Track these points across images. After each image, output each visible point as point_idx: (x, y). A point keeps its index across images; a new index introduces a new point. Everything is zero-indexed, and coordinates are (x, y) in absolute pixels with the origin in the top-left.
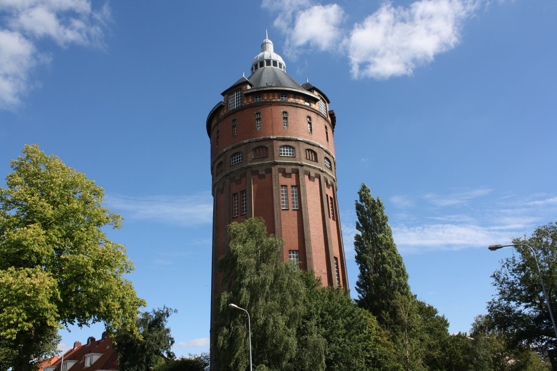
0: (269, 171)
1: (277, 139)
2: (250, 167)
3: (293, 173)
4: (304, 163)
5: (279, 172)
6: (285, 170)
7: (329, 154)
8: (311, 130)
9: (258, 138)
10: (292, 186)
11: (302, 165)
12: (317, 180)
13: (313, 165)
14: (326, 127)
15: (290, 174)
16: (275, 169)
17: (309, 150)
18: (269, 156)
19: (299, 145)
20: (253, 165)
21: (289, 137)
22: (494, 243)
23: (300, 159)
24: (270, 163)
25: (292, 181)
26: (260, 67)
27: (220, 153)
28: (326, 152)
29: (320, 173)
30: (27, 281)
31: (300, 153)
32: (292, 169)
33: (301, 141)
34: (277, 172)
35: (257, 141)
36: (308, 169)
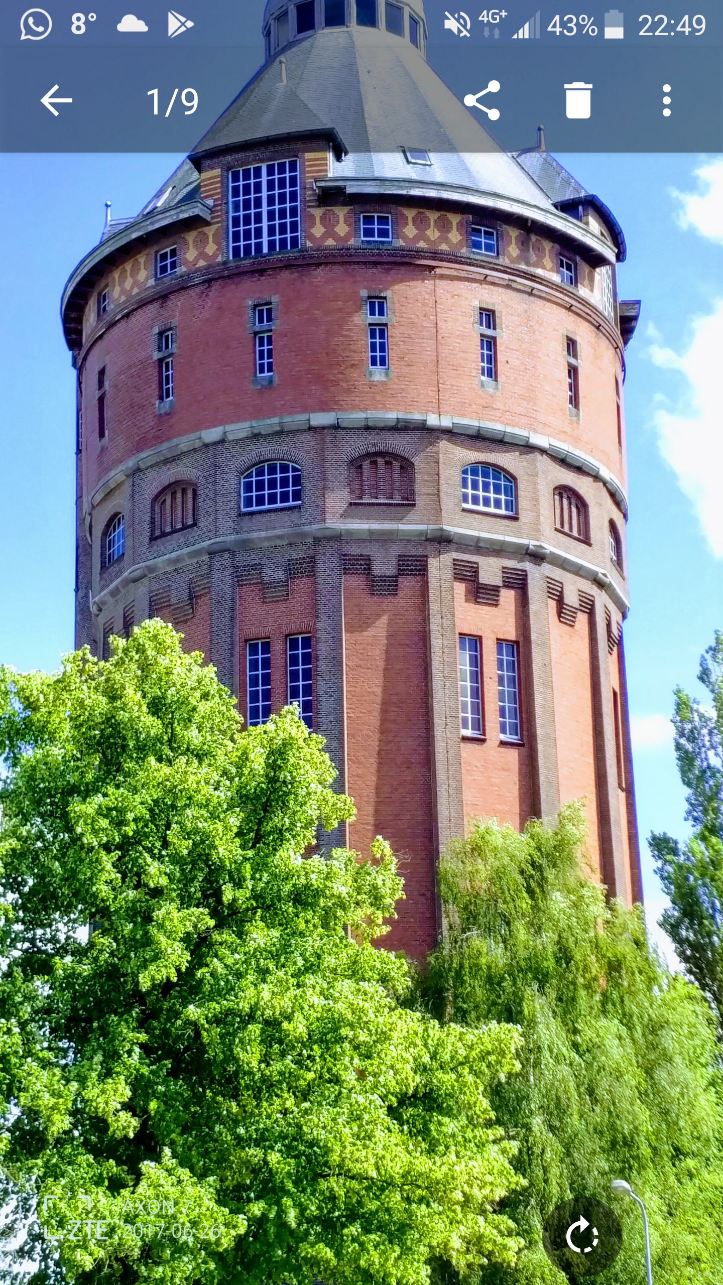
0: (414, 567)
1: (450, 434)
2: (337, 537)
3: (507, 585)
5: (458, 577)
6: (476, 571)
7: (580, 469)
8: (575, 400)
10: (500, 641)
11: (538, 557)
12: (582, 619)
14: (571, 345)
15: (496, 589)
16: (440, 567)
17: (372, 456)
18: (420, 501)
19: (533, 463)
20: (349, 532)
21: (499, 427)
22: (108, 373)
23: (536, 531)
24: (421, 533)
25: (496, 622)
28: (563, 461)
29: (594, 590)
30: (361, 1003)
31: (536, 500)
33: (543, 451)
34: (448, 574)
36: (557, 573)
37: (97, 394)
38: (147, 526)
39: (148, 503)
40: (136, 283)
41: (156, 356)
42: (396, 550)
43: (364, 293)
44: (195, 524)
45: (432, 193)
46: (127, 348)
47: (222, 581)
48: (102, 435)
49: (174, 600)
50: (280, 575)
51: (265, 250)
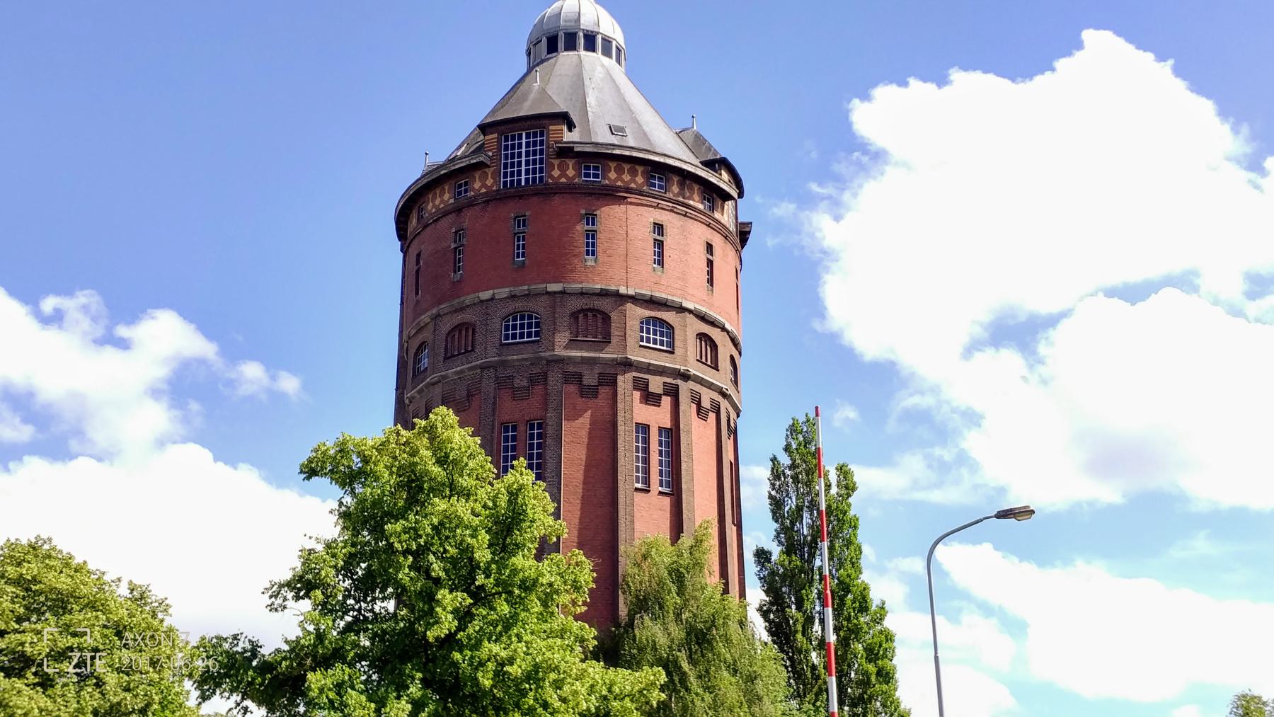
1: (635, 299)
2: (561, 360)
3: (666, 394)
5: (636, 388)
7: (713, 323)
8: (711, 281)
9: (590, 286)
11: (686, 377)
12: (712, 416)
14: (710, 248)
15: (660, 396)
16: (624, 381)
17: (585, 311)
18: (614, 340)
20: (570, 358)
24: (613, 359)
25: (659, 417)
26: (567, 49)
27: (468, 299)
33: (690, 311)
34: (630, 386)
35: (583, 294)
36: (698, 388)
40: (442, 202)
41: (453, 246)
42: (597, 370)
43: (583, 212)
47: (488, 385)
48: (417, 293)
50: (525, 383)
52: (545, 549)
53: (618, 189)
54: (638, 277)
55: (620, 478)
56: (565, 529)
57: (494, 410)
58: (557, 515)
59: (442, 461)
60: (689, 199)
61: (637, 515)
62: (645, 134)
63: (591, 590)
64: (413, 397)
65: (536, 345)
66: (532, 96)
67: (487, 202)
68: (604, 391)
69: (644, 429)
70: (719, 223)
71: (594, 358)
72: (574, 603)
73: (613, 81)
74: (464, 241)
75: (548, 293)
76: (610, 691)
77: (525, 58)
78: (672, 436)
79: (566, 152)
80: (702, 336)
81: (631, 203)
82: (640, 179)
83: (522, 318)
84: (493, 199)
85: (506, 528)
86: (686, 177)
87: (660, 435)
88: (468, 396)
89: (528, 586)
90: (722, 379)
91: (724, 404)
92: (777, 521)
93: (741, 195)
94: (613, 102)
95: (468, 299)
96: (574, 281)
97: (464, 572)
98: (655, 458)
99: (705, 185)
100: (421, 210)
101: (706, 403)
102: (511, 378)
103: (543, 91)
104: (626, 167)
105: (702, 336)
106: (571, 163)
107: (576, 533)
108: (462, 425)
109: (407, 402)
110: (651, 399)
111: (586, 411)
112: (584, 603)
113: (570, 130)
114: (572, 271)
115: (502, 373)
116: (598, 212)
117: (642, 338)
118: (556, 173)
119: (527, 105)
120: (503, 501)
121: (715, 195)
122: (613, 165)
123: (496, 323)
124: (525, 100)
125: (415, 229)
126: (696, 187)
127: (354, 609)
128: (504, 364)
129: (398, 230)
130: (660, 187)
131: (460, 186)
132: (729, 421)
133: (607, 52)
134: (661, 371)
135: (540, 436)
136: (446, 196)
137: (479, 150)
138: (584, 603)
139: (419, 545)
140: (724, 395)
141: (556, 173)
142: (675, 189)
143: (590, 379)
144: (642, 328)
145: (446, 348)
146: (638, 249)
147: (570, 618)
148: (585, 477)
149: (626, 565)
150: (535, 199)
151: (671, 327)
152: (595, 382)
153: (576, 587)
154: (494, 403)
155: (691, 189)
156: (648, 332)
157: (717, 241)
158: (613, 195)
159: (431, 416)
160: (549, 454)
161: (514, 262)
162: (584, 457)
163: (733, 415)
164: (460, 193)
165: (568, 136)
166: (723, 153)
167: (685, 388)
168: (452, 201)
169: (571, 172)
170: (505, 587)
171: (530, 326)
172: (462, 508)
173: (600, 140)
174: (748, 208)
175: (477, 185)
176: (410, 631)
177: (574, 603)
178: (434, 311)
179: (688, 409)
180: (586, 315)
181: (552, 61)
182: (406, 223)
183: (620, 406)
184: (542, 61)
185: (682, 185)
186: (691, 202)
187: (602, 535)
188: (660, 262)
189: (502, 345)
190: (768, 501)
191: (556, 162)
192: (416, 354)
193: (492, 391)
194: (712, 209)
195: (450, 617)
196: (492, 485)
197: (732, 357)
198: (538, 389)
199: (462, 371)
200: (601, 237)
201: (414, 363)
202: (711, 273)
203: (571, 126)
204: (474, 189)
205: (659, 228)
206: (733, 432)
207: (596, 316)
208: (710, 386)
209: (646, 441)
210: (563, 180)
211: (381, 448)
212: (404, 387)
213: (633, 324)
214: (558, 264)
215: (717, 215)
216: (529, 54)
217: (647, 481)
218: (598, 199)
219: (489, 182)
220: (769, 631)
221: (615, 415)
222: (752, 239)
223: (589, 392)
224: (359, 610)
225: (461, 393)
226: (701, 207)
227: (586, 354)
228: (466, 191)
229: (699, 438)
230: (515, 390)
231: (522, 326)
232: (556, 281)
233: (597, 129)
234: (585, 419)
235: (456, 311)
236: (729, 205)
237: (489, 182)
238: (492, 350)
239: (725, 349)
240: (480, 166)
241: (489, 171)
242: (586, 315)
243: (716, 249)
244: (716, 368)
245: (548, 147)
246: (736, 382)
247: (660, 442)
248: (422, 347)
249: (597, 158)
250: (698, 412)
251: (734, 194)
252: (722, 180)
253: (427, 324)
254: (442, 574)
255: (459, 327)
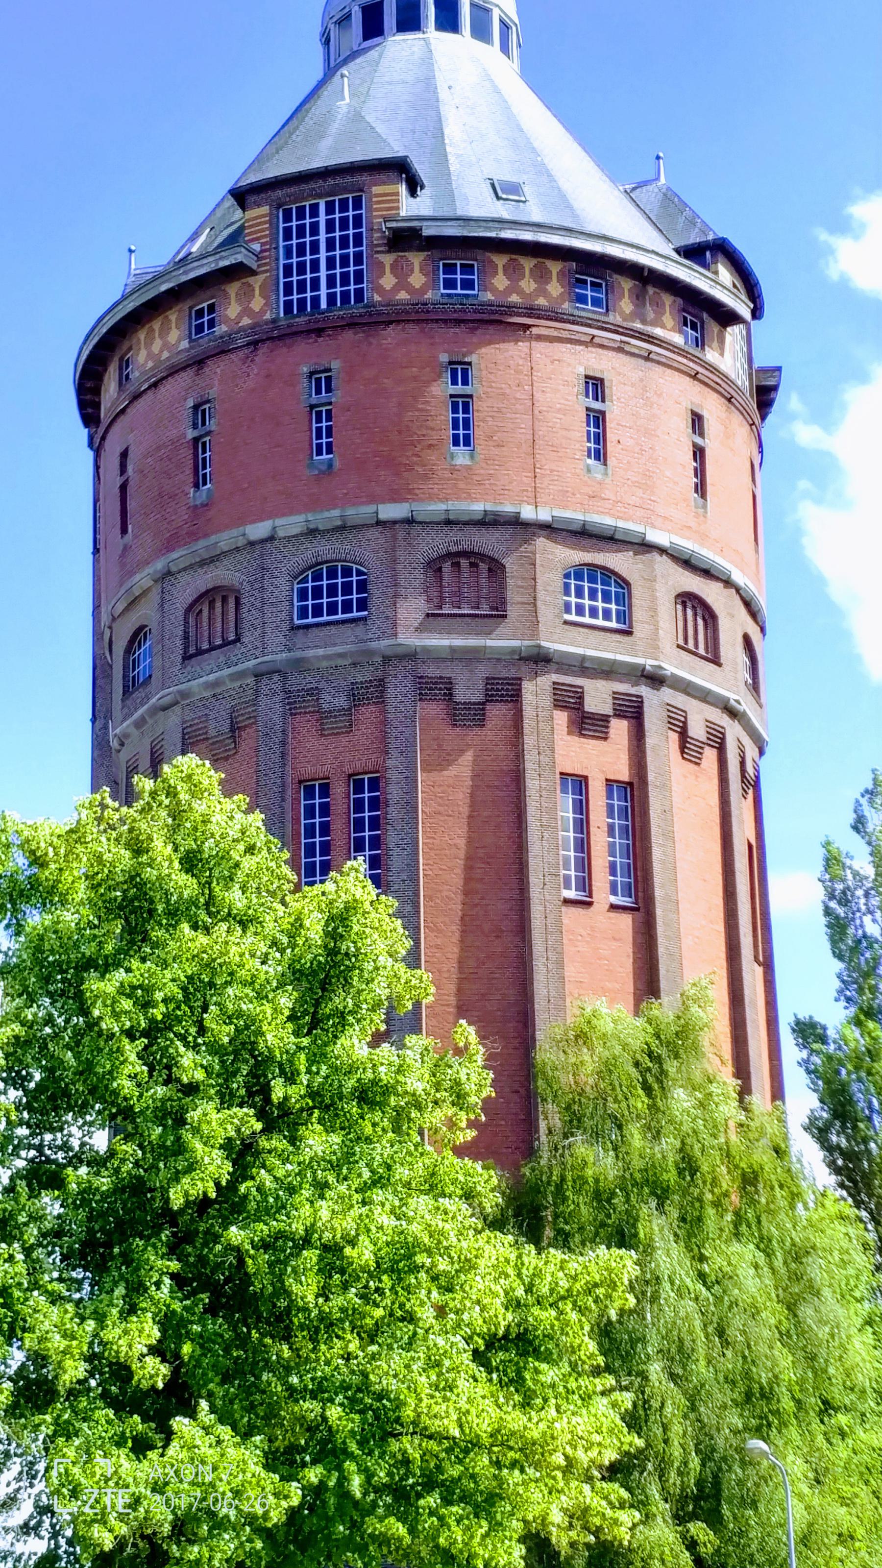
0: (506, 692)
1: (549, 529)
2: (411, 656)
3: (619, 714)
4: (670, 668)
7: (707, 573)
8: (701, 488)
10: (609, 783)
11: (656, 680)
12: (710, 755)
13: (700, 674)
14: (697, 421)
15: (604, 720)
16: (536, 692)
17: (454, 557)
18: (512, 611)
20: (426, 650)
23: (654, 648)
24: (513, 651)
25: (604, 759)
27: (225, 539)
31: (653, 610)
32: (616, 696)
33: (662, 551)
34: (547, 700)
36: (680, 700)
37: (119, 481)
38: (179, 642)
39: (180, 613)
40: (165, 346)
41: (191, 434)
42: (483, 671)
43: (444, 358)
44: (238, 640)
45: (527, 236)
46: (155, 425)
47: (271, 708)
48: (124, 530)
49: (212, 733)
50: (342, 701)
51: (324, 305)
52: (397, 1026)
53: (512, 310)
54: (565, 489)
55: (535, 880)
56: (424, 986)
57: (283, 755)
58: (413, 960)
59: (191, 862)
60: (654, 324)
61: (569, 949)
62: (563, 197)
63: (486, 1101)
64: (126, 735)
65: (359, 629)
66: (335, 127)
67: (255, 344)
68: (497, 712)
69: (579, 784)
70: (712, 369)
71: (475, 650)
72: (451, 1124)
73: (497, 91)
74: (212, 425)
75: (379, 523)
76: (529, 1290)
77: (319, 49)
78: (632, 794)
79: (405, 239)
80: (688, 600)
81: (539, 338)
82: (555, 288)
83: (332, 574)
84: (263, 338)
85: (322, 981)
86: (646, 279)
87: (610, 796)
88: (233, 730)
89: (369, 1096)
90: (727, 681)
91: (733, 731)
92: (840, 957)
93: (757, 313)
94: (483, 125)
95: (225, 539)
96: (431, 498)
97: (248, 1073)
98: (600, 840)
99: (695, 296)
100: (125, 364)
101: (697, 731)
102: (314, 693)
103: (357, 117)
104: (528, 263)
105: (687, 599)
106: (416, 259)
107: (452, 988)
108: (228, 789)
109: (114, 744)
110: (587, 724)
111: (462, 752)
112: (471, 1124)
113: (413, 193)
114: (426, 477)
115: (297, 682)
116: (473, 358)
117: (567, 608)
118: (388, 281)
119: (326, 144)
120: (315, 929)
121: (704, 314)
122: (500, 260)
123: (282, 588)
124: (321, 136)
125: (114, 404)
126: (668, 300)
127: (30, 1147)
128: (299, 665)
129: (82, 405)
130: (596, 302)
131: (200, 314)
132: (743, 763)
133: (481, 32)
134: (607, 671)
135: (375, 804)
136: (174, 336)
137: (233, 240)
138: (471, 1124)
139: (152, 1021)
140: (733, 713)
141: (388, 281)
142: (626, 305)
143: (469, 690)
144: (567, 587)
145: (186, 637)
146: (569, 431)
147: (448, 1153)
148: (467, 880)
149: (546, 1054)
150: (348, 335)
151: (624, 583)
152: (477, 696)
153: (459, 1098)
154: (284, 743)
155: (658, 305)
156: (579, 594)
157: (713, 408)
158: (498, 321)
159: (166, 768)
160: (392, 838)
161: (311, 465)
162: (462, 843)
163: (751, 752)
164: (200, 329)
165: (409, 207)
166: (720, 229)
167: (655, 703)
168: (185, 344)
169: (407, 280)
170: (325, 1104)
171: (347, 589)
172: (239, 949)
173: (474, 212)
174: (774, 339)
175: (233, 310)
176: (136, 1189)
177: (451, 1124)
178: (159, 565)
179: (660, 742)
180: (457, 565)
181: (373, 54)
182: (97, 391)
183: (529, 741)
184: (354, 55)
185: (639, 297)
186: (658, 332)
187: (501, 993)
188: (600, 455)
189: (294, 628)
190: (823, 920)
191: (387, 259)
192: (129, 651)
193: (277, 719)
194: (700, 343)
195: (217, 1154)
196: (283, 903)
197: (747, 642)
198: (368, 713)
199: (216, 683)
200: (481, 408)
201: (125, 668)
202: (700, 472)
203: (414, 185)
204: (227, 320)
205: (595, 386)
206: (753, 785)
207: (474, 565)
208: (705, 696)
209: (582, 807)
210: (403, 295)
211: (75, 835)
212: (109, 715)
213: (549, 581)
214: (395, 462)
215: (711, 355)
216: (327, 42)
217: (585, 884)
218: (473, 330)
219: (257, 303)
220: (832, 1165)
221: (519, 756)
222: (780, 398)
223: (472, 716)
224: (40, 1148)
225: (217, 727)
226: (678, 339)
227: (458, 642)
228: (212, 324)
229: (683, 797)
230: (322, 716)
231: (332, 591)
232: (395, 497)
233: (465, 190)
234: (463, 768)
235: (204, 563)
236: (734, 334)
237: (257, 303)
238: (276, 638)
239: (733, 623)
240: (237, 272)
241: (256, 282)
242: (457, 565)
243: (711, 424)
244: (715, 660)
245: (371, 230)
246: (755, 687)
247: (610, 809)
248: (139, 635)
249: (463, 250)
250: (683, 748)
251: (744, 311)
252: (718, 284)
253: (145, 592)
254: (200, 1075)
255: (209, 596)
